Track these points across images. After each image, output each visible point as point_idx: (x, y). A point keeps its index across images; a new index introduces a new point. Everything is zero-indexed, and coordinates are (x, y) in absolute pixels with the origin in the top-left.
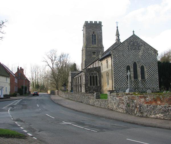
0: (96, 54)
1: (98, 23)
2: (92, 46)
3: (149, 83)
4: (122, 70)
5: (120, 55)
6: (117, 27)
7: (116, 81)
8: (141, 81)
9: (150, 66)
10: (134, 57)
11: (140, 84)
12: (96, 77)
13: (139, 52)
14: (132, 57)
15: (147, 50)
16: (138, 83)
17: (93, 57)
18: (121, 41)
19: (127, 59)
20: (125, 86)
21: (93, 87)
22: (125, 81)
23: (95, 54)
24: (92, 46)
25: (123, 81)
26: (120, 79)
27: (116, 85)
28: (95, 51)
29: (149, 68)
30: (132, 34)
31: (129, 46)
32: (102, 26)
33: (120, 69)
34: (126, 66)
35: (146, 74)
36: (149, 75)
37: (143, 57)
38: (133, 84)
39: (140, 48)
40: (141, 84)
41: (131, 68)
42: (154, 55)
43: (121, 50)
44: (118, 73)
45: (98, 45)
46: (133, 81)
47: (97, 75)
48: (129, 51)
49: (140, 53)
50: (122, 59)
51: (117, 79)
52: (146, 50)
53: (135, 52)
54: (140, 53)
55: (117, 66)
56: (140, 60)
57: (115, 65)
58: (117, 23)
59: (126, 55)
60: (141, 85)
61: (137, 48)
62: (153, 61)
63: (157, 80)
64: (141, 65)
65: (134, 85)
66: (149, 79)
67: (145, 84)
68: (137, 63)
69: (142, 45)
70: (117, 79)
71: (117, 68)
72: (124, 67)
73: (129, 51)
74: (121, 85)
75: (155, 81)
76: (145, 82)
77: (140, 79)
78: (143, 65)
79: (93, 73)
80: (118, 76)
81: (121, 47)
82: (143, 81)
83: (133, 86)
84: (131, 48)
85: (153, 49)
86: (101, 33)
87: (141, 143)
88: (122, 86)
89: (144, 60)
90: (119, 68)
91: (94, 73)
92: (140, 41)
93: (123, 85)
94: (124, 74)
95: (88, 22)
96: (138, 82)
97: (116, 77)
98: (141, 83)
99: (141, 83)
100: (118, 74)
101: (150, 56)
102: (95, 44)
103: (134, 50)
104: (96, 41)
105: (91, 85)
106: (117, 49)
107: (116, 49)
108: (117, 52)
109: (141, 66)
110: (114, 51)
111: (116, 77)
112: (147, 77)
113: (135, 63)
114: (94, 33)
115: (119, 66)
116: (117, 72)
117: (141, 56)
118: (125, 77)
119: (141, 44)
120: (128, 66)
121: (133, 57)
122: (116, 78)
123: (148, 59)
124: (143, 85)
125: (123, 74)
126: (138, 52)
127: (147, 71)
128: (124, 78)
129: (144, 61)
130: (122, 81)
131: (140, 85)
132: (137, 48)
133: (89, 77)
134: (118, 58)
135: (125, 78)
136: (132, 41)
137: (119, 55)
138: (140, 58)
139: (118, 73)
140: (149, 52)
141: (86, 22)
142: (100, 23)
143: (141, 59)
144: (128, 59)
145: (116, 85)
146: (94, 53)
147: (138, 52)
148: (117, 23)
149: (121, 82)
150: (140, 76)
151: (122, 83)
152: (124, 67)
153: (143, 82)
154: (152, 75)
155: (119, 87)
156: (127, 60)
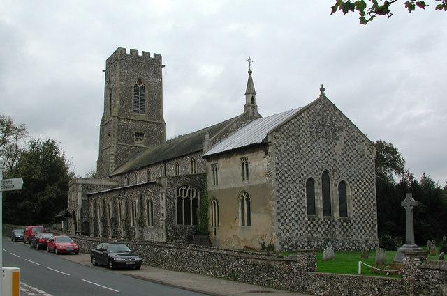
0: (144, 138)
1: (152, 56)
3: (356, 228)
4: (295, 190)
6: (250, 72)
7: (282, 217)
8: (340, 221)
11: (337, 230)
15: (354, 142)
20: (302, 231)
25: (299, 218)
26: (290, 212)
27: (282, 228)
29: (358, 188)
30: (317, 95)
33: (292, 187)
35: (351, 204)
36: (356, 206)
37: (345, 159)
40: (340, 230)
42: (368, 156)
45: (150, 116)
46: (322, 220)
47: (196, 196)
48: (313, 140)
49: (339, 148)
51: (285, 212)
52: (352, 141)
54: (339, 148)
55: (284, 178)
58: (249, 60)
59: (307, 150)
64: (341, 180)
65: (324, 232)
67: (349, 230)
70: (285, 212)
71: (284, 184)
72: (300, 182)
73: (313, 140)
74: (293, 228)
75: (370, 223)
76: (349, 224)
78: (345, 180)
79: (185, 190)
83: (322, 232)
84: (317, 133)
85: (366, 141)
86: (160, 84)
91: (189, 190)
92: (339, 116)
93: (299, 228)
95: (149, 54)
98: (340, 227)
99: (340, 227)
100: (287, 200)
101: (359, 157)
102: (143, 111)
105: (180, 222)
106: (285, 131)
109: (339, 182)
110: (277, 135)
113: (326, 172)
114: (140, 81)
115: (289, 179)
116: (284, 195)
117: (340, 156)
120: (343, 181)
121: (322, 157)
122: (281, 209)
123: (356, 166)
130: (296, 219)
131: (337, 233)
133: (176, 201)
134: (286, 154)
135: (304, 210)
136: (319, 115)
143: (340, 164)
145: (282, 228)
146: (140, 135)
148: (249, 60)
150: (338, 207)
151: (296, 225)
152: (300, 182)
153: (344, 224)
154: (363, 206)
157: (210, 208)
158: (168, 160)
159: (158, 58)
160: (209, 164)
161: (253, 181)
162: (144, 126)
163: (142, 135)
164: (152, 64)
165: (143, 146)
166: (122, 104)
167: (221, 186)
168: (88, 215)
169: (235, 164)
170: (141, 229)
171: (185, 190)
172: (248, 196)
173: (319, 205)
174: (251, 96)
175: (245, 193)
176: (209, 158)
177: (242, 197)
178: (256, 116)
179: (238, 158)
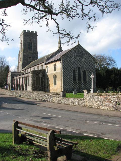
0: (31, 59)
1: (34, 32)
3: (89, 85)
5: (68, 60)
9: (90, 71)
10: (79, 63)
11: (83, 85)
12: (42, 78)
13: (83, 59)
14: (77, 63)
16: (81, 84)
17: (29, 61)
18: (62, 49)
19: (73, 64)
20: (71, 86)
21: (38, 86)
22: (72, 82)
26: (67, 80)
31: (75, 54)
32: (38, 35)
34: (72, 70)
38: (78, 85)
39: (83, 56)
40: (83, 85)
41: (76, 71)
43: (69, 56)
44: (66, 76)
49: (83, 60)
50: (70, 64)
51: (66, 80)
53: (79, 58)
54: (83, 60)
56: (83, 66)
57: (65, 69)
60: (83, 86)
61: (81, 56)
62: (93, 67)
63: (95, 82)
64: (84, 70)
65: (78, 86)
66: (89, 81)
67: (87, 86)
68: (80, 68)
69: (85, 54)
70: (66, 80)
77: (82, 81)
78: (85, 70)
80: (66, 78)
81: (69, 54)
82: (85, 83)
83: (78, 86)
84: (76, 56)
86: (37, 41)
87: (91, 136)
88: (69, 86)
89: (86, 66)
90: (67, 72)
93: (70, 85)
94: (71, 76)
95: (26, 31)
96: (81, 83)
97: (65, 78)
98: (83, 84)
99: (83, 84)
100: (66, 77)
103: (78, 57)
104: (32, 47)
107: (65, 55)
108: (66, 58)
109: (83, 70)
110: (64, 56)
111: (65, 78)
112: (88, 79)
113: (79, 68)
116: (65, 75)
117: (84, 63)
118: (72, 79)
119: (84, 52)
120: (74, 70)
121: (78, 63)
122: (65, 79)
124: (85, 86)
125: (70, 77)
126: (82, 59)
127: (88, 74)
128: (71, 79)
129: (86, 67)
131: (83, 86)
132: (81, 56)
133: (36, 78)
135: (72, 80)
136: (77, 50)
137: (67, 60)
138: (83, 64)
139: (66, 76)
140: (89, 59)
141: (25, 31)
142: (36, 33)
144: (74, 64)
145: (65, 85)
147: (82, 59)
149: (68, 83)
150: (83, 78)
155: (67, 87)
156: (73, 65)
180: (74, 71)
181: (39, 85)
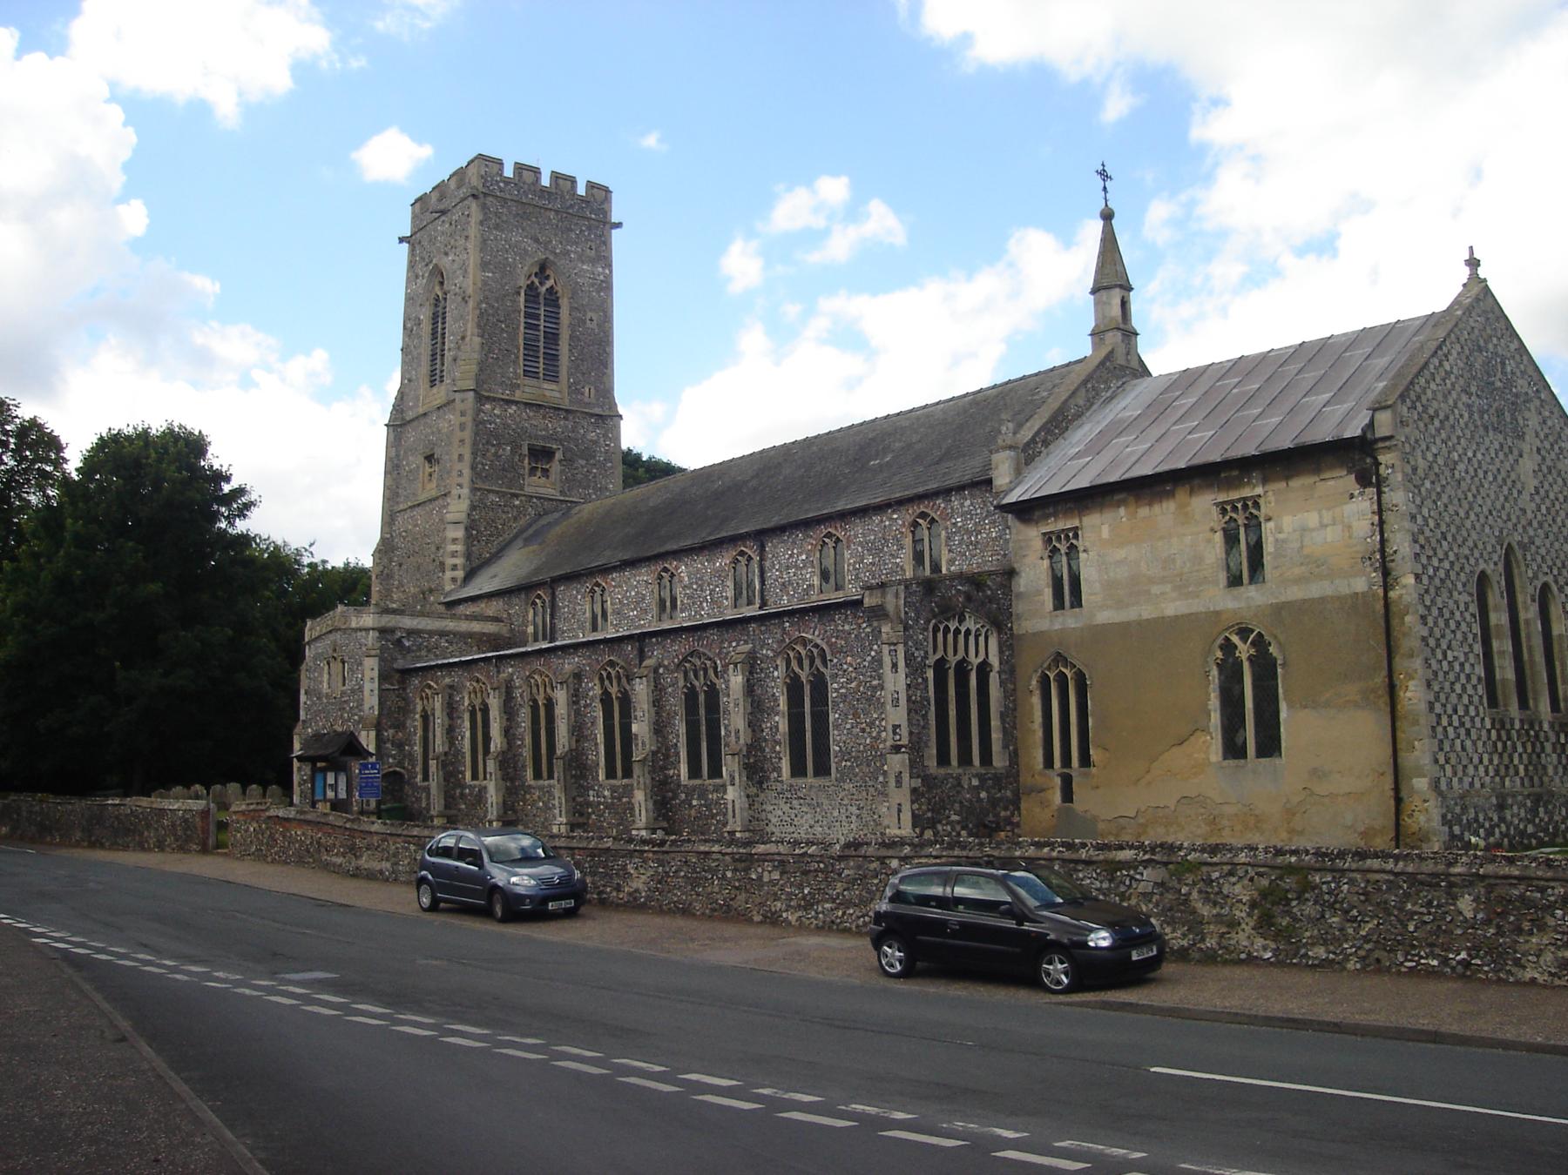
0: (555, 467)
2: (528, 390)
12: (984, 669)
17: (528, 490)
21: (958, 779)
23: (546, 472)
24: (528, 390)
28: (544, 438)
32: (619, 225)
45: (574, 389)
49: (1528, 465)
58: (1104, 175)
79: (957, 631)
86: (606, 286)
91: (968, 632)
102: (552, 376)
105: (943, 759)
114: (543, 270)
119: (1521, 385)
133: (930, 674)
146: (541, 454)
148: (1104, 175)
157: (1036, 701)
158: (780, 530)
159: (600, 195)
160: (1031, 537)
161: (1281, 585)
162: (557, 425)
163: (548, 454)
164: (581, 215)
165: (550, 492)
166: (487, 347)
167: (1099, 608)
168: (400, 745)
169: (1190, 531)
170: (754, 790)
171: (957, 631)
172: (1260, 643)
173: (1506, 671)
174: (1116, 296)
175: (1244, 632)
176: (1026, 511)
177: (1228, 647)
178: (1134, 364)
179: (1204, 504)
180: (1483, 579)
181: (965, 759)
